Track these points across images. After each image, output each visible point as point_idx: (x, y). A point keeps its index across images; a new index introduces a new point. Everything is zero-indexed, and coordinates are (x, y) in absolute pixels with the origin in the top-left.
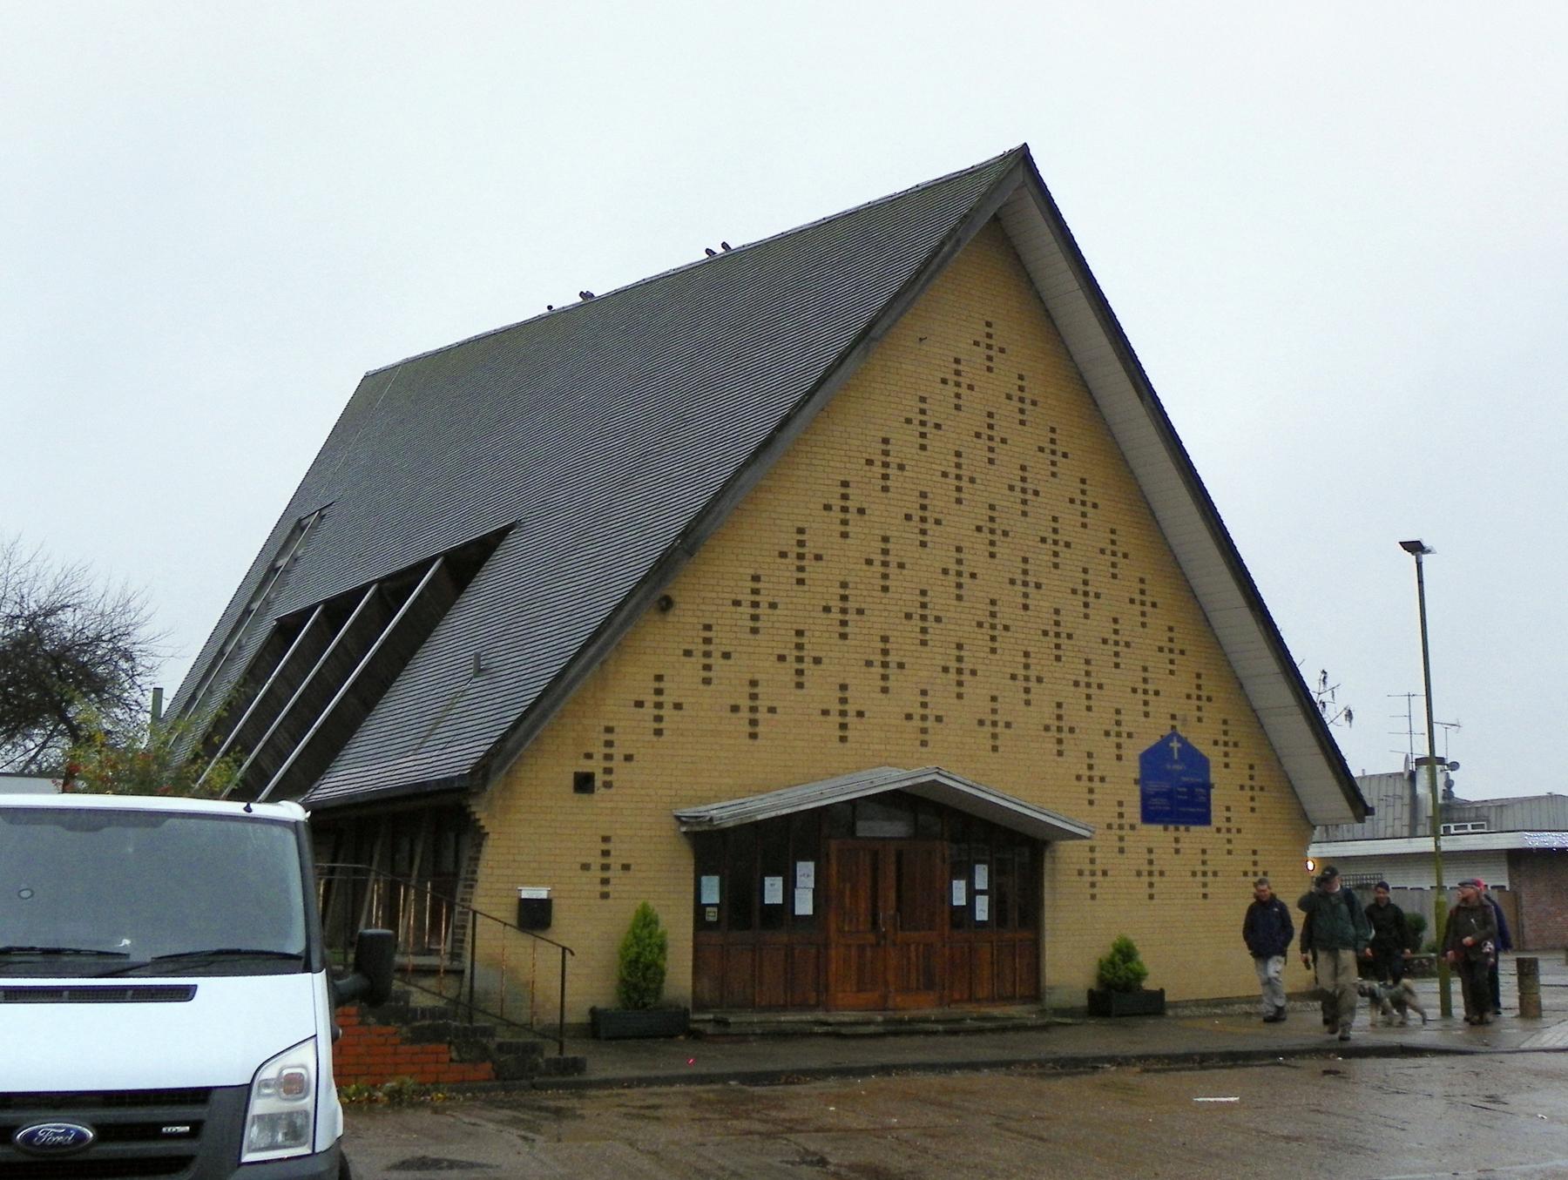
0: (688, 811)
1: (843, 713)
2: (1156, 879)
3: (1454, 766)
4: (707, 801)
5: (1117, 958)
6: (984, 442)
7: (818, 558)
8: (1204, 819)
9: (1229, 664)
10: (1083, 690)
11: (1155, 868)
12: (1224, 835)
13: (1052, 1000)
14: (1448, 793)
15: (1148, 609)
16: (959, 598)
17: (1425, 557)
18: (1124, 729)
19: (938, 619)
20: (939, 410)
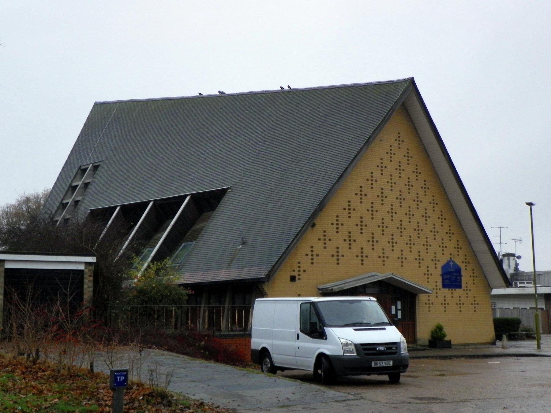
0: (321, 287)
1: (362, 256)
2: (446, 306)
3: (519, 257)
4: (325, 283)
5: (438, 330)
6: (398, 171)
7: (354, 210)
8: (460, 287)
9: (467, 237)
10: (426, 247)
11: (446, 302)
12: (466, 292)
13: (419, 343)
14: (516, 269)
15: (443, 220)
16: (392, 220)
17: (533, 207)
18: (437, 259)
19: (387, 227)
20: (386, 162)
